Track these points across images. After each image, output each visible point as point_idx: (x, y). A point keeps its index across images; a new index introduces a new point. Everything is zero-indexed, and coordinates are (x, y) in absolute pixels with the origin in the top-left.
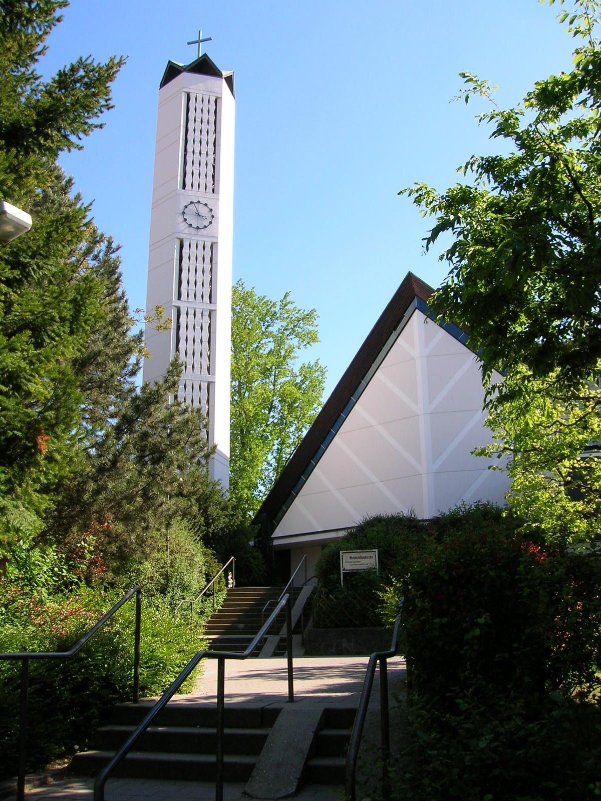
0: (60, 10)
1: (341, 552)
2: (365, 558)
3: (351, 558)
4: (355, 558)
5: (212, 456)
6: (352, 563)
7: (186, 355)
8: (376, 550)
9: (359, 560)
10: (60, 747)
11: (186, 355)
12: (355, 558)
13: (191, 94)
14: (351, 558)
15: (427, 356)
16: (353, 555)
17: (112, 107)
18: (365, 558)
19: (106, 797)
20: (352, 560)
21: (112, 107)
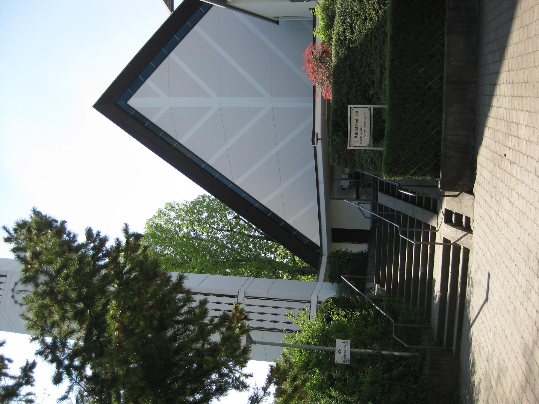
0: (69, 385)
1: (349, 148)
2: (357, 120)
3: (356, 137)
4: (357, 132)
5: (44, 282)
6: (363, 135)
7: (251, 305)
8: (349, 106)
9: (359, 128)
10: (102, 340)
11: (251, 305)
12: (357, 132)
13: (6, 277)
14: (356, 137)
15: (169, 96)
16: (353, 135)
17: (219, 400)
18: (357, 120)
19: (1, 284)
20: (359, 136)
21: (219, 400)
